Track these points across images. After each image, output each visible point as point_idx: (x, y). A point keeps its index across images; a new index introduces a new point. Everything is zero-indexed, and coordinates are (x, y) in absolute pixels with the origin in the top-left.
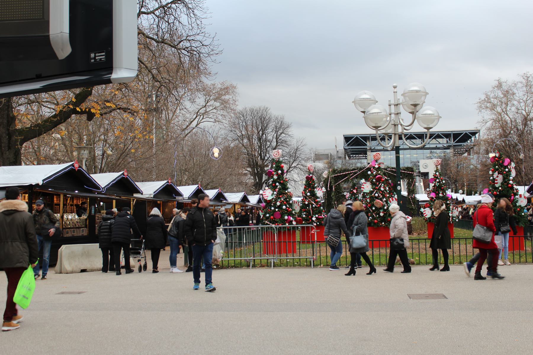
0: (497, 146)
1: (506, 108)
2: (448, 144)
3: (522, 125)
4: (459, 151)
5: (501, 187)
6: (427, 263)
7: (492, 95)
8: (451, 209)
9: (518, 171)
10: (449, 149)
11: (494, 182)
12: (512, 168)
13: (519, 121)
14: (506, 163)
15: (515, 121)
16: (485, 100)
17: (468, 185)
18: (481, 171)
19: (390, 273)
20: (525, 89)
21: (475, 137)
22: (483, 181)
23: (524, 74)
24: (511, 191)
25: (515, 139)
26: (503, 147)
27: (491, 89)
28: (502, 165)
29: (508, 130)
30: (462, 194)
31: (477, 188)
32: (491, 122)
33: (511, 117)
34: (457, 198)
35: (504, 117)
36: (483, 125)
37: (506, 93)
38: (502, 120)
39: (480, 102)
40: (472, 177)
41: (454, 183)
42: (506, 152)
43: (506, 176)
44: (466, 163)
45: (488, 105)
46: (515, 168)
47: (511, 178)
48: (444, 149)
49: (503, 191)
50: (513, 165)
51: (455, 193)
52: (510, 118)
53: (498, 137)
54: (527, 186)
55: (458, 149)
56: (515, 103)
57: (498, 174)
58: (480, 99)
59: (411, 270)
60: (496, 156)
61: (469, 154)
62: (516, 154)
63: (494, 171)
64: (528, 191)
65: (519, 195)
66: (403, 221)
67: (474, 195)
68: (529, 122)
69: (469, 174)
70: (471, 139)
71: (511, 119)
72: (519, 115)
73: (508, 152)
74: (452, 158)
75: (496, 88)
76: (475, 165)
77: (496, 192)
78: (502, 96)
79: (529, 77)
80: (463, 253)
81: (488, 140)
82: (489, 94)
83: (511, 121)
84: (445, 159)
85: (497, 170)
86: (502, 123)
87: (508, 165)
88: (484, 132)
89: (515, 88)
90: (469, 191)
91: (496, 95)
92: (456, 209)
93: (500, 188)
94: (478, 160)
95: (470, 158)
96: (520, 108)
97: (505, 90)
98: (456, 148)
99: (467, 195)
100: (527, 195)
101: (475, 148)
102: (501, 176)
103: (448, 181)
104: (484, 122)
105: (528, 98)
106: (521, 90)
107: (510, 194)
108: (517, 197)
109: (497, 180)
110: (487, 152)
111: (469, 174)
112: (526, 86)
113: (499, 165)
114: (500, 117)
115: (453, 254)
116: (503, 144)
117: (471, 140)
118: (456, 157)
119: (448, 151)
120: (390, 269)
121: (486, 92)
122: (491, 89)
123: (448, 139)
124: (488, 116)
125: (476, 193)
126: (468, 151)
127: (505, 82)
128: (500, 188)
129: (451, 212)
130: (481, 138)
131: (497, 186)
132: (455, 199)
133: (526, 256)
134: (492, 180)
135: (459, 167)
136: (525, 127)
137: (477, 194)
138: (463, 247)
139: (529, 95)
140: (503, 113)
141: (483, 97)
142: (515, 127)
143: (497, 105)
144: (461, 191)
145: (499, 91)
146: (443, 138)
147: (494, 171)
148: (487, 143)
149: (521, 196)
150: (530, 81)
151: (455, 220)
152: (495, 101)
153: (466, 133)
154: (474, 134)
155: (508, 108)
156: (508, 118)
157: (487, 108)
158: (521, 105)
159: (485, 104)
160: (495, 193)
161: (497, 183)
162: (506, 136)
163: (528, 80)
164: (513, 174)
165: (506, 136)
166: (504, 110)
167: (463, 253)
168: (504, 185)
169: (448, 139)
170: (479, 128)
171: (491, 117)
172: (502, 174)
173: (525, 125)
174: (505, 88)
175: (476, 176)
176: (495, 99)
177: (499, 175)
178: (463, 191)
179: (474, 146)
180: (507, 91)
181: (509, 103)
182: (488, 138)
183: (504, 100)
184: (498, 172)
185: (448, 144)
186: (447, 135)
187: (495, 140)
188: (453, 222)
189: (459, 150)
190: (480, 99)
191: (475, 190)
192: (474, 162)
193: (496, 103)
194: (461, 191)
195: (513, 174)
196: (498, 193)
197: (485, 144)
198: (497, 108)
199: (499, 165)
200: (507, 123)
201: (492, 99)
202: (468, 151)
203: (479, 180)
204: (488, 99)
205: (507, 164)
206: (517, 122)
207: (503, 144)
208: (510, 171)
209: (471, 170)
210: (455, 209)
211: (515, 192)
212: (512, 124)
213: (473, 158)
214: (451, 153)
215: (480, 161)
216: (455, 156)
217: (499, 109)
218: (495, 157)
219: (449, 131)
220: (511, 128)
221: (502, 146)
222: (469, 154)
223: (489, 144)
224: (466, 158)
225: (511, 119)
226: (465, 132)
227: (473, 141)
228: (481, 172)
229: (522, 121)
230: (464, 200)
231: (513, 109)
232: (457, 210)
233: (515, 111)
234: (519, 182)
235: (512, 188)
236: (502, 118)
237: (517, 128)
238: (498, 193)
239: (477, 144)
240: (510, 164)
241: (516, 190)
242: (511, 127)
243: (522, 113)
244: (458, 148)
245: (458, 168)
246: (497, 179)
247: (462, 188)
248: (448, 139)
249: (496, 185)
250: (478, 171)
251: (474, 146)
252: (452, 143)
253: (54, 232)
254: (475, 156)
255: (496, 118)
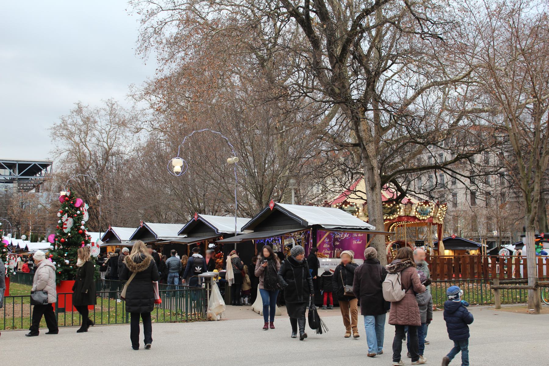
0: (71, 183)
1: (85, 139)
2: (11, 177)
3: (102, 160)
4: (25, 186)
5: (70, 233)
6: (72, 325)
7: (69, 121)
8: (7, 259)
9: (95, 215)
10: (12, 183)
11: (62, 227)
12: (84, 210)
13: (99, 154)
14: (78, 205)
15: (95, 154)
16: (61, 125)
17: (33, 230)
18: (51, 212)
19: (84, 333)
20: (108, 117)
21: (46, 170)
22: (52, 224)
23: (109, 100)
24: (82, 237)
25: (94, 176)
26: (79, 184)
27: (69, 114)
28: (72, 206)
29: (86, 164)
30: (25, 240)
31: (44, 233)
32: (66, 153)
33: (90, 149)
34: (18, 245)
35: (82, 148)
36: (56, 156)
37: (87, 121)
38: (80, 153)
39: (54, 128)
40: (39, 219)
41: (17, 225)
42: (81, 191)
43: (77, 220)
44: (34, 201)
45: (65, 132)
46: (88, 211)
47: (83, 222)
48: (6, 182)
49: (72, 238)
50: (86, 207)
51: (17, 238)
52: (89, 150)
53: (74, 172)
54: (104, 232)
55: (24, 183)
56: (96, 133)
57: (68, 217)
58: (55, 124)
59: (39, 332)
60: (67, 194)
61: (38, 191)
62: (93, 194)
63: (63, 214)
64: (103, 240)
65: (91, 243)
66: (48, 271)
67: (40, 242)
68: (110, 157)
69: (36, 216)
70: (41, 172)
71: (90, 152)
72: (99, 147)
73: (84, 191)
74: (15, 195)
75: (75, 113)
76: (44, 205)
77: (64, 238)
78: (82, 123)
79: (114, 104)
80: (18, 315)
81: (62, 175)
82: (66, 119)
83: (90, 154)
84: (6, 195)
85: (67, 212)
86: (80, 155)
87: (80, 206)
88: (57, 164)
89: (98, 116)
90: (34, 237)
91: (75, 122)
92: (15, 259)
93: (69, 234)
94: (47, 199)
95: (38, 195)
96: (102, 140)
97: (86, 117)
98: (21, 182)
99: (31, 242)
100: (101, 243)
101: (45, 184)
102: (71, 220)
103: (8, 223)
104: (58, 152)
105: (112, 129)
106: (104, 118)
107: (80, 242)
108: (88, 245)
109: (66, 224)
110: (60, 189)
111: (36, 216)
112: (110, 114)
113: (70, 206)
114: (77, 148)
115: (5, 316)
116: (80, 182)
117: (41, 173)
118: (20, 193)
119: (11, 185)
120: (34, 332)
121: (63, 117)
122: (69, 114)
123: (12, 171)
124: (64, 145)
125: (43, 239)
126: (37, 187)
127: (86, 107)
128: (69, 234)
129: (7, 263)
130: (54, 171)
131: (66, 231)
132: (16, 246)
133: (94, 316)
134: (60, 224)
135: (24, 206)
136: (106, 163)
137: (43, 241)
138: (18, 308)
139: (112, 125)
140: (81, 144)
141: (59, 122)
142: (94, 162)
143: (75, 133)
144: (24, 237)
145: (79, 117)
146: (5, 168)
147: (63, 214)
148: (61, 179)
149: (93, 244)
150: (114, 109)
151: (12, 273)
152: (73, 129)
153: (35, 164)
154: (45, 166)
155: (88, 139)
156: (86, 150)
157: (63, 135)
158: (103, 137)
159: (61, 130)
160: (62, 239)
161: (66, 228)
162: (83, 172)
163: (112, 107)
164: (86, 217)
165: (83, 172)
166: (83, 140)
167: (18, 315)
168: (74, 230)
169: (12, 170)
170: (51, 160)
171: (67, 148)
172: (72, 217)
173: (106, 160)
174: (85, 114)
175: (44, 219)
176: (73, 126)
177: (69, 218)
178: (27, 236)
179: (44, 181)
180: (88, 118)
181: (89, 133)
182: (62, 172)
183: (83, 128)
184: (68, 215)
185: (11, 177)
186: (11, 166)
187: (70, 175)
188: (9, 276)
189: (25, 185)
190: (55, 124)
191: (42, 235)
192: (42, 200)
193: (74, 130)
194: (24, 237)
195: (86, 217)
196: (66, 240)
197: (58, 180)
198: (75, 137)
199: (70, 206)
200: (85, 156)
201: (69, 126)
202: (37, 187)
203: (48, 223)
204: (64, 125)
205: (79, 206)
206: (97, 155)
207: (80, 182)
208: (82, 214)
209: (39, 210)
210: (13, 259)
211: (87, 239)
212: (91, 158)
213: (42, 196)
214: (14, 189)
215: (50, 201)
216: (19, 192)
217: (77, 139)
218: (66, 196)
219: (13, 161)
220: (90, 163)
221: (78, 183)
222: (38, 191)
223: (62, 179)
224: (33, 195)
225: (90, 152)
226: (34, 163)
227: (43, 175)
228: (51, 214)
229: (103, 155)
230: (27, 248)
231: (94, 140)
232: (16, 261)
233: (95, 143)
234: (95, 227)
235: (83, 234)
236: (79, 149)
237: (97, 162)
238: (66, 240)
239: (48, 178)
240: (82, 206)
241: (88, 236)
242: (90, 161)
243: (103, 146)
244: (24, 182)
245: (22, 207)
246: (66, 222)
247: (25, 232)
248: (12, 171)
249: (64, 230)
250: (48, 212)
251: (44, 181)
252: (17, 175)
253: (247, 267)
254: (45, 194)
255: (73, 149)
